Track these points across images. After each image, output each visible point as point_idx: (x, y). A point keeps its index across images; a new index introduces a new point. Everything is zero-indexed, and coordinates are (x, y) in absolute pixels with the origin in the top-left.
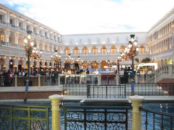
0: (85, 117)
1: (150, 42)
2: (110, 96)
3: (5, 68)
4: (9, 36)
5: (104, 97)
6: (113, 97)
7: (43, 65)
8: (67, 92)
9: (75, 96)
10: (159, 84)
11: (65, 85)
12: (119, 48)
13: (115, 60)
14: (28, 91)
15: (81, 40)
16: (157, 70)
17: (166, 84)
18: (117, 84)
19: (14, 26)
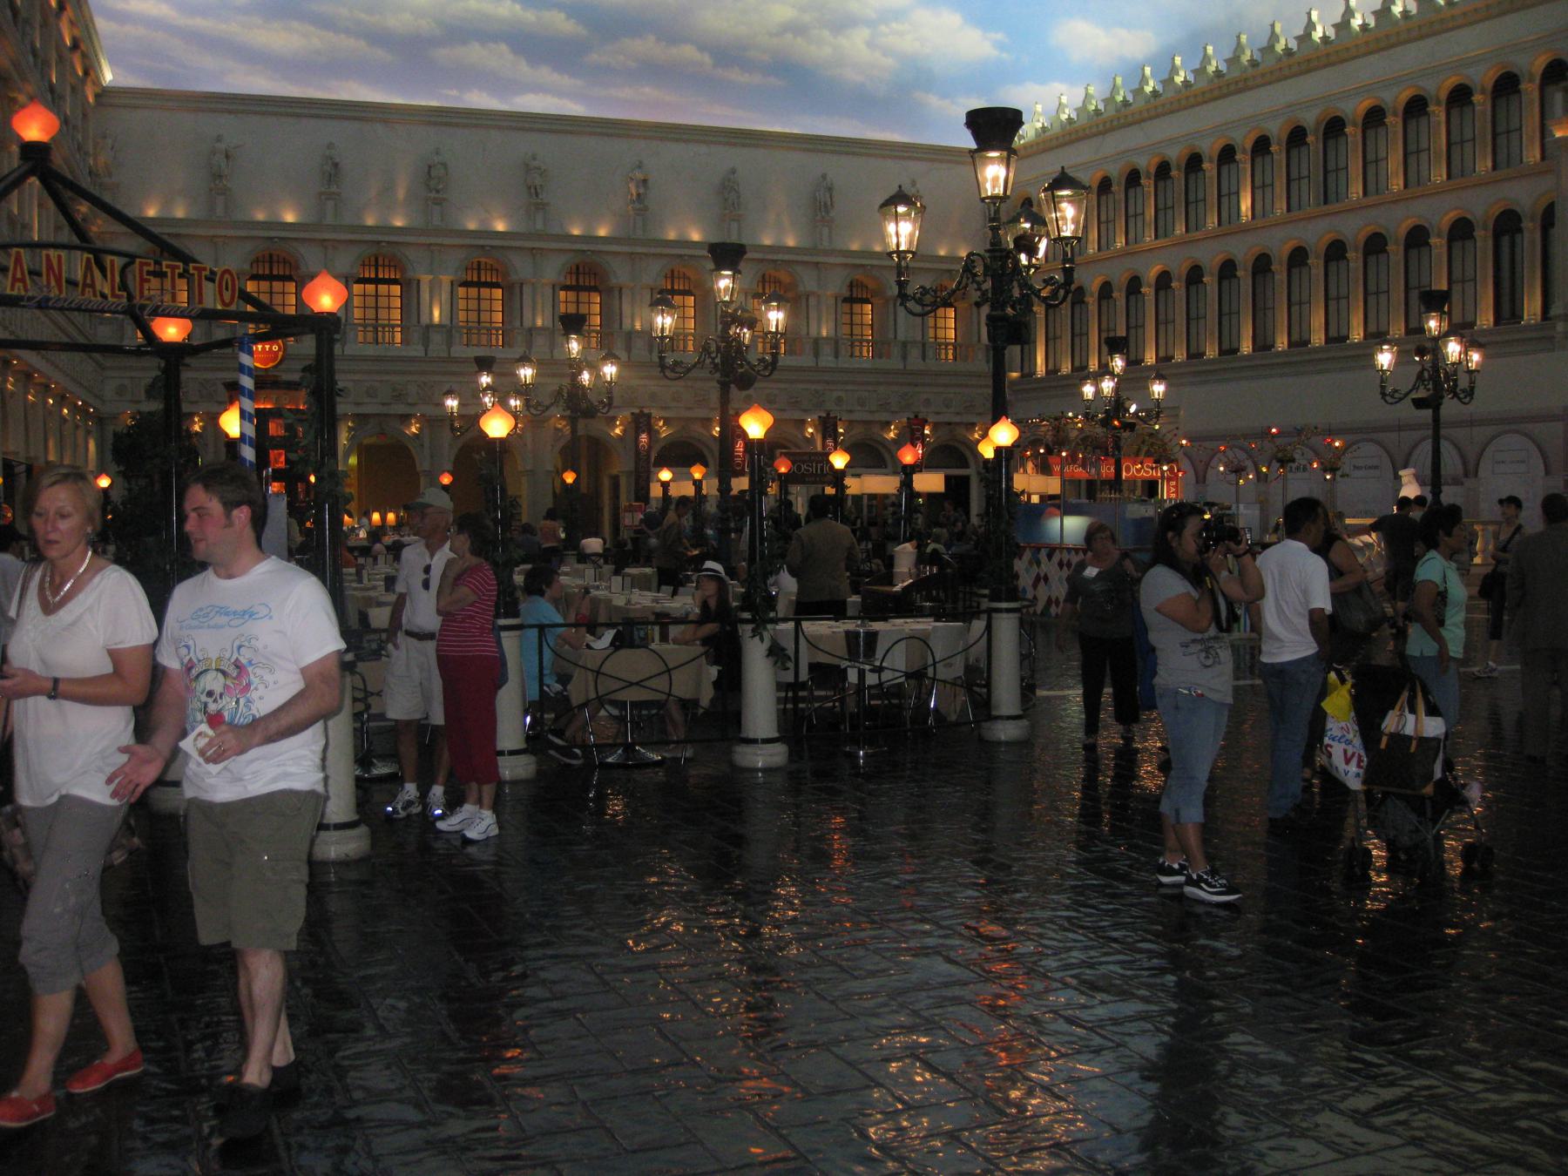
12: (446, 279)
15: (332, 172)
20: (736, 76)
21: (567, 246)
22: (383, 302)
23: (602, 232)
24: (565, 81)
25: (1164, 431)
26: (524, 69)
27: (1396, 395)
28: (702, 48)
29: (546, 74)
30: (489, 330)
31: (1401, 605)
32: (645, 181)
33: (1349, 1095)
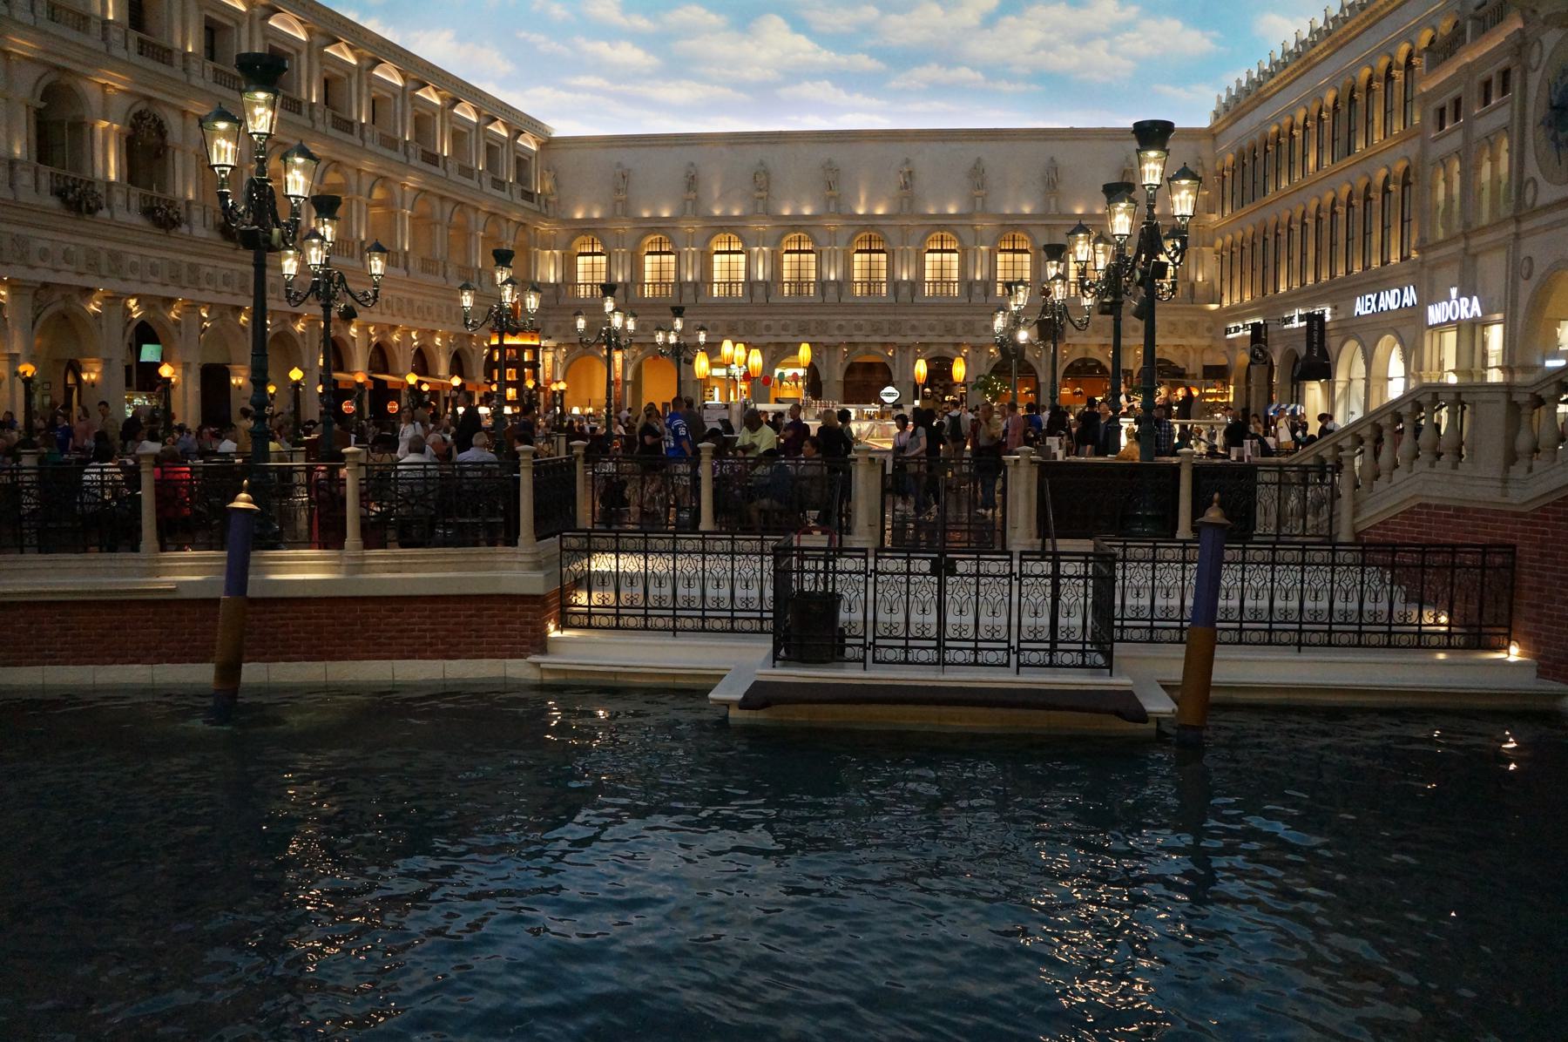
0: (589, 597)
1: (1228, 211)
2: (976, 650)
3: (25, 373)
4: (120, 133)
5: (923, 656)
6: (1002, 656)
7: (401, 369)
8: (595, 599)
9: (1290, 654)
10: (1393, 548)
11: (574, 543)
13: (949, 339)
14: (250, 594)
16: (1366, 432)
17: (1454, 549)
18: (1021, 535)
19: (164, 54)
20: (1003, 86)
21: (854, 222)
22: (1018, 266)
23: (952, 210)
24: (874, 103)
25: (483, 331)
26: (843, 97)
27: (299, 298)
28: (974, 68)
29: (859, 99)
30: (948, 282)
31: (620, 453)
32: (910, 172)
33: (610, 824)
